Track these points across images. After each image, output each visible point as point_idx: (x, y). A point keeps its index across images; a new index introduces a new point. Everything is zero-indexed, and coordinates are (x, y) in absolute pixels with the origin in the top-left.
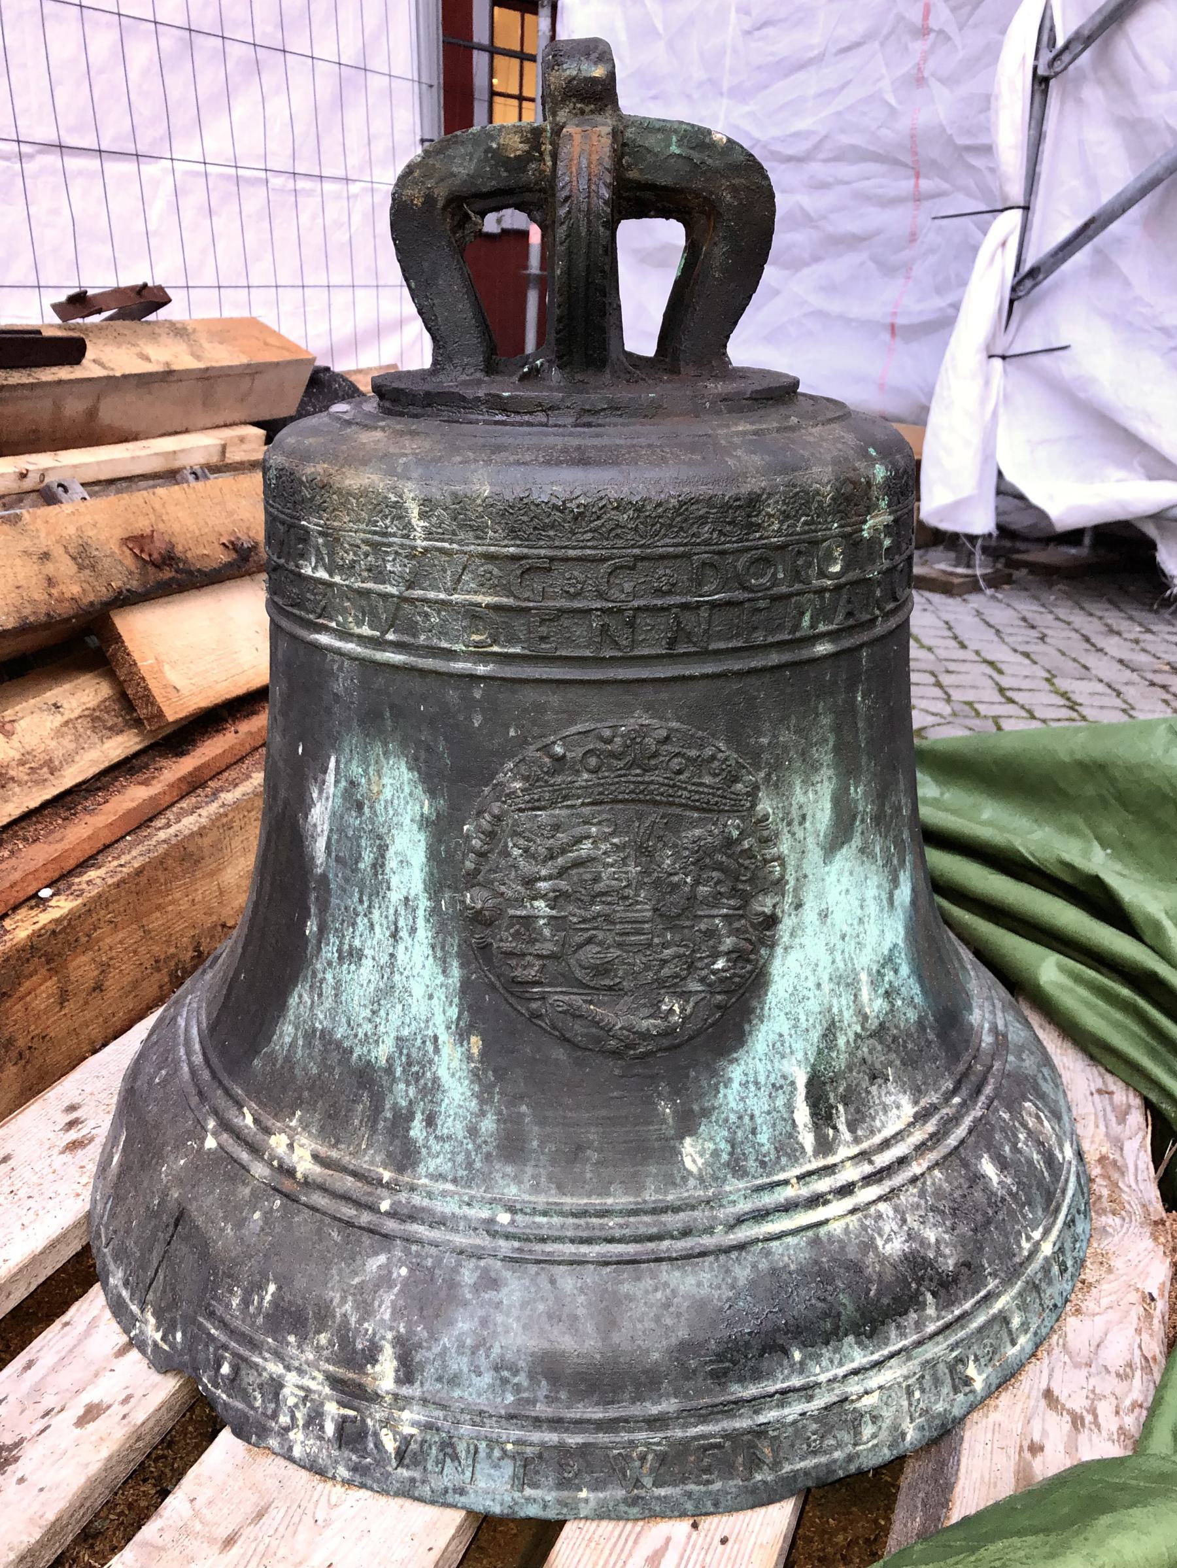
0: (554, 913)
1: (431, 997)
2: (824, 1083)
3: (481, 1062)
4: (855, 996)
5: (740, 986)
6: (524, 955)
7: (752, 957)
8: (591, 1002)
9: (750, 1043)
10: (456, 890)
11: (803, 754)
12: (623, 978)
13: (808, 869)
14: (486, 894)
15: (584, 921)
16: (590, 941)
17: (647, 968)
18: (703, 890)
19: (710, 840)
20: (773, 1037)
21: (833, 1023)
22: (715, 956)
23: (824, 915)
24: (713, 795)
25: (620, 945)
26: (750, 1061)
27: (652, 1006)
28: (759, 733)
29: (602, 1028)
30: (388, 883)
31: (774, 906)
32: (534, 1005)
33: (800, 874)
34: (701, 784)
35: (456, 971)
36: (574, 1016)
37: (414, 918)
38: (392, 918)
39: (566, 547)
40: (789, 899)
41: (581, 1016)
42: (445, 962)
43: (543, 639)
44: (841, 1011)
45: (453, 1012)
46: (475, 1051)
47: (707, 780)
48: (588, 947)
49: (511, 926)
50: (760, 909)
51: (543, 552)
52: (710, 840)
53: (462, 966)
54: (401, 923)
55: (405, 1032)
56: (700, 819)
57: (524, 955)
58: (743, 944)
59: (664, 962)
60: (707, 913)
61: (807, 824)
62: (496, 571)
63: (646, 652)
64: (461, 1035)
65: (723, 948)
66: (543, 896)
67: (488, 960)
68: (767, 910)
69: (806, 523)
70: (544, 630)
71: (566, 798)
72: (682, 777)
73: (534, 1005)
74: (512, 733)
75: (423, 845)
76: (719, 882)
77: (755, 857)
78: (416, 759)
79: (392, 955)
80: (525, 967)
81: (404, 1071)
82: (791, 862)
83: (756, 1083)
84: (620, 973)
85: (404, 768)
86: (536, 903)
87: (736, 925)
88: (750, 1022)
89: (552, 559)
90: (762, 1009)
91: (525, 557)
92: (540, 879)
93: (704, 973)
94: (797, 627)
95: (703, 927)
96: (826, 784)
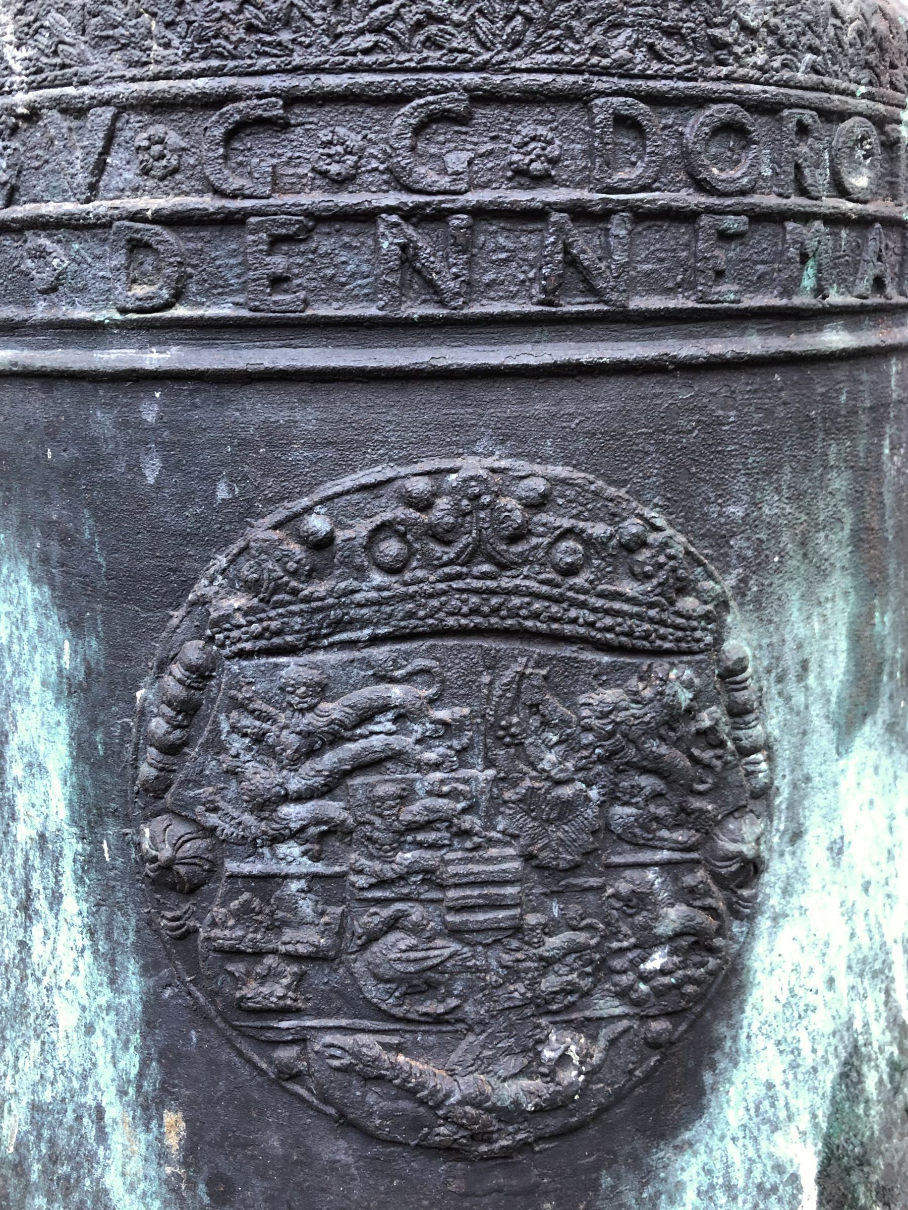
0: (319, 868)
1: (90, 1030)
2: (848, 1170)
3: (185, 1164)
4: (887, 992)
5: (697, 999)
6: (259, 954)
7: (719, 942)
8: (399, 1048)
9: (713, 1109)
10: (128, 820)
11: (803, 544)
12: (464, 998)
13: (813, 766)
14: (180, 829)
15: (382, 883)
16: (393, 924)
17: (513, 973)
18: (622, 812)
19: (635, 710)
20: (756, 1091)
21: (856, 1047)
22: (647, 944)
23: (837, 850)
24: (639, 616)
25: (455, 933)
26: (715, 1143)
27: (525, 1051)
28: (725, 495)
29: (422, 1102)
30: (12, 807)
31: (757, 841)
32: (285, 1054)
33: (799, 775)
34: (618, 596)
35: (134, 982)
36: (367, 1079)
37: (58, 874)
38: (20, 873)
39: (317, 69)
40: (780, 823)
41: (380, 1078)
42: (113, 962)
43: (278, 282)
44: (866, 1025)
45: (131, 1062)
46: (173, 1141)
47: (629, 588)
48: (391, 938)
49: (232, 894)
50: (732, 847)
51: (267, 83)
52: (635, 710)
53: (146, 970)
54: (36, 884)
55: (47, 1096)
56: (614, 668)
57: (259, 954)
58: (702, 918)
59: (547, 963)
60: (630, 858)
61: (811, 680)
62: (174, 138)
63: (496, 308)
64: (145, 1108)
65: (664, 928)
66: (295, 835)
67: (193, 965)
68: (747, 849)
69: (814, 69)
70: (279, 262)
71: (339, 625)
72: (579, 580)
73: (285, 1054)
74: (222, 492)
75: (63, 732)
76: (656, 796)
77: (722, 744)
78: (45, 560)
79: (22, 944)
80: (263, 979)
81: (44, 1172)
82: (784, 753)
83: (729, 1187)
84: (458, 987)
85: (25, 582)
86: (283, 849)
87: (689, 880)
88: (713, 1066)
89: (292, 99)
90: (735, 1039)
91: (232, 96)
92: (286, 798)
93: (625, 980)
94: (790, 287)
95: (624, 887)
96: (840, 604)
